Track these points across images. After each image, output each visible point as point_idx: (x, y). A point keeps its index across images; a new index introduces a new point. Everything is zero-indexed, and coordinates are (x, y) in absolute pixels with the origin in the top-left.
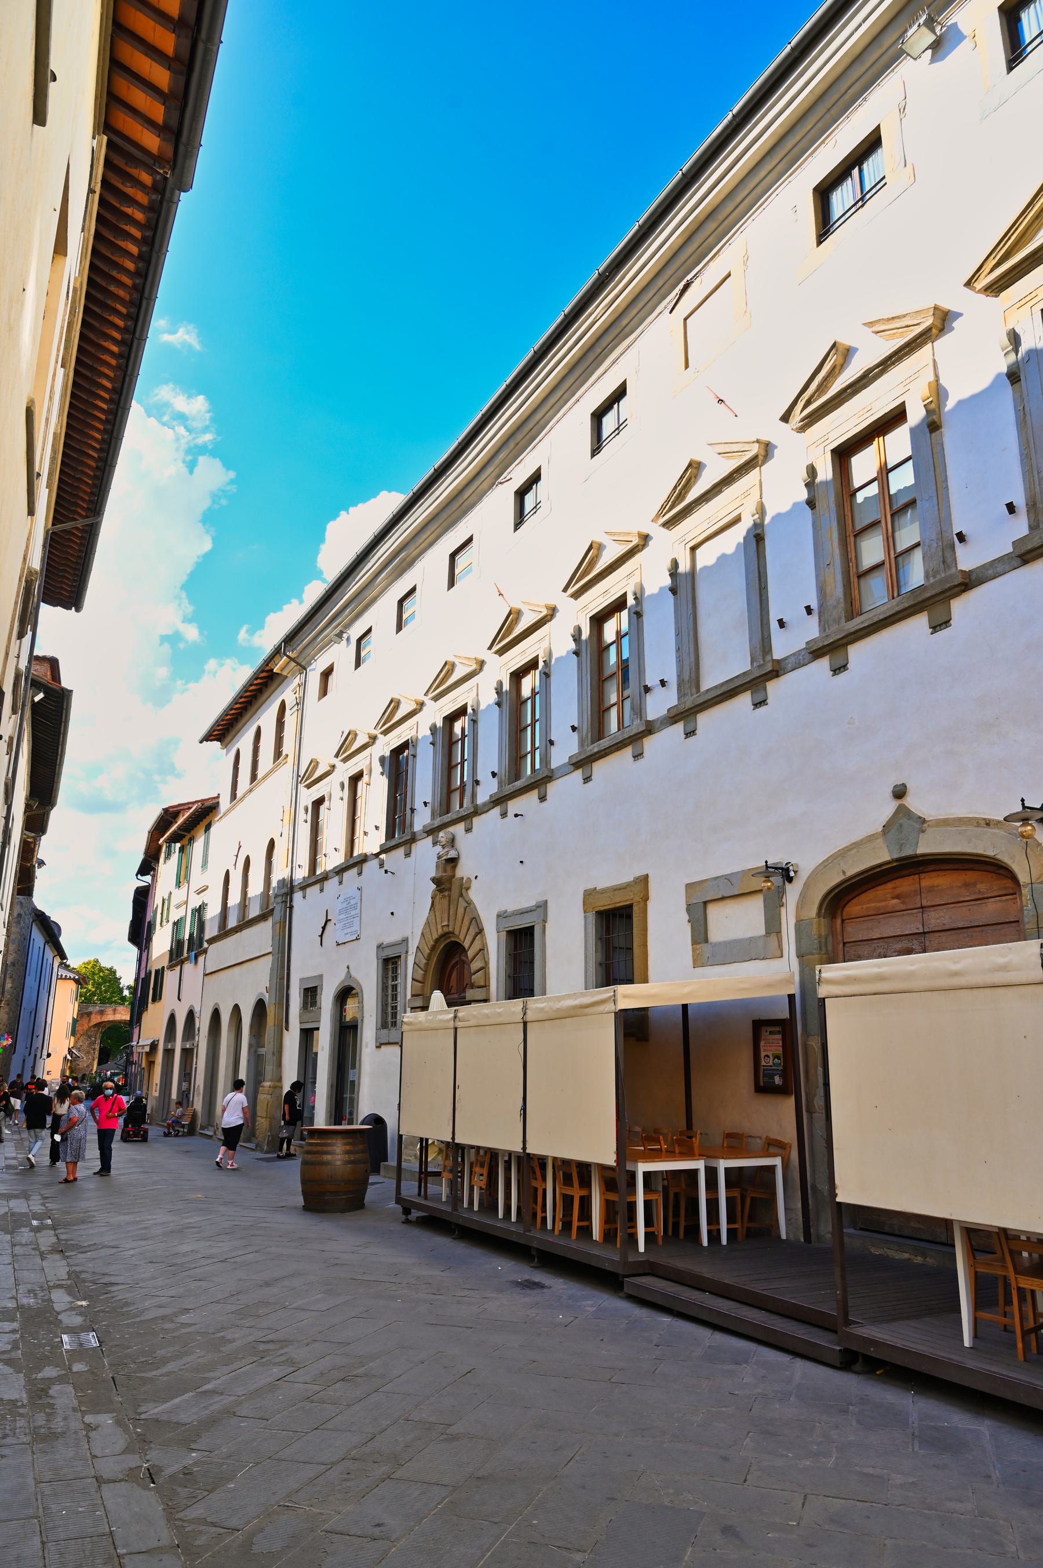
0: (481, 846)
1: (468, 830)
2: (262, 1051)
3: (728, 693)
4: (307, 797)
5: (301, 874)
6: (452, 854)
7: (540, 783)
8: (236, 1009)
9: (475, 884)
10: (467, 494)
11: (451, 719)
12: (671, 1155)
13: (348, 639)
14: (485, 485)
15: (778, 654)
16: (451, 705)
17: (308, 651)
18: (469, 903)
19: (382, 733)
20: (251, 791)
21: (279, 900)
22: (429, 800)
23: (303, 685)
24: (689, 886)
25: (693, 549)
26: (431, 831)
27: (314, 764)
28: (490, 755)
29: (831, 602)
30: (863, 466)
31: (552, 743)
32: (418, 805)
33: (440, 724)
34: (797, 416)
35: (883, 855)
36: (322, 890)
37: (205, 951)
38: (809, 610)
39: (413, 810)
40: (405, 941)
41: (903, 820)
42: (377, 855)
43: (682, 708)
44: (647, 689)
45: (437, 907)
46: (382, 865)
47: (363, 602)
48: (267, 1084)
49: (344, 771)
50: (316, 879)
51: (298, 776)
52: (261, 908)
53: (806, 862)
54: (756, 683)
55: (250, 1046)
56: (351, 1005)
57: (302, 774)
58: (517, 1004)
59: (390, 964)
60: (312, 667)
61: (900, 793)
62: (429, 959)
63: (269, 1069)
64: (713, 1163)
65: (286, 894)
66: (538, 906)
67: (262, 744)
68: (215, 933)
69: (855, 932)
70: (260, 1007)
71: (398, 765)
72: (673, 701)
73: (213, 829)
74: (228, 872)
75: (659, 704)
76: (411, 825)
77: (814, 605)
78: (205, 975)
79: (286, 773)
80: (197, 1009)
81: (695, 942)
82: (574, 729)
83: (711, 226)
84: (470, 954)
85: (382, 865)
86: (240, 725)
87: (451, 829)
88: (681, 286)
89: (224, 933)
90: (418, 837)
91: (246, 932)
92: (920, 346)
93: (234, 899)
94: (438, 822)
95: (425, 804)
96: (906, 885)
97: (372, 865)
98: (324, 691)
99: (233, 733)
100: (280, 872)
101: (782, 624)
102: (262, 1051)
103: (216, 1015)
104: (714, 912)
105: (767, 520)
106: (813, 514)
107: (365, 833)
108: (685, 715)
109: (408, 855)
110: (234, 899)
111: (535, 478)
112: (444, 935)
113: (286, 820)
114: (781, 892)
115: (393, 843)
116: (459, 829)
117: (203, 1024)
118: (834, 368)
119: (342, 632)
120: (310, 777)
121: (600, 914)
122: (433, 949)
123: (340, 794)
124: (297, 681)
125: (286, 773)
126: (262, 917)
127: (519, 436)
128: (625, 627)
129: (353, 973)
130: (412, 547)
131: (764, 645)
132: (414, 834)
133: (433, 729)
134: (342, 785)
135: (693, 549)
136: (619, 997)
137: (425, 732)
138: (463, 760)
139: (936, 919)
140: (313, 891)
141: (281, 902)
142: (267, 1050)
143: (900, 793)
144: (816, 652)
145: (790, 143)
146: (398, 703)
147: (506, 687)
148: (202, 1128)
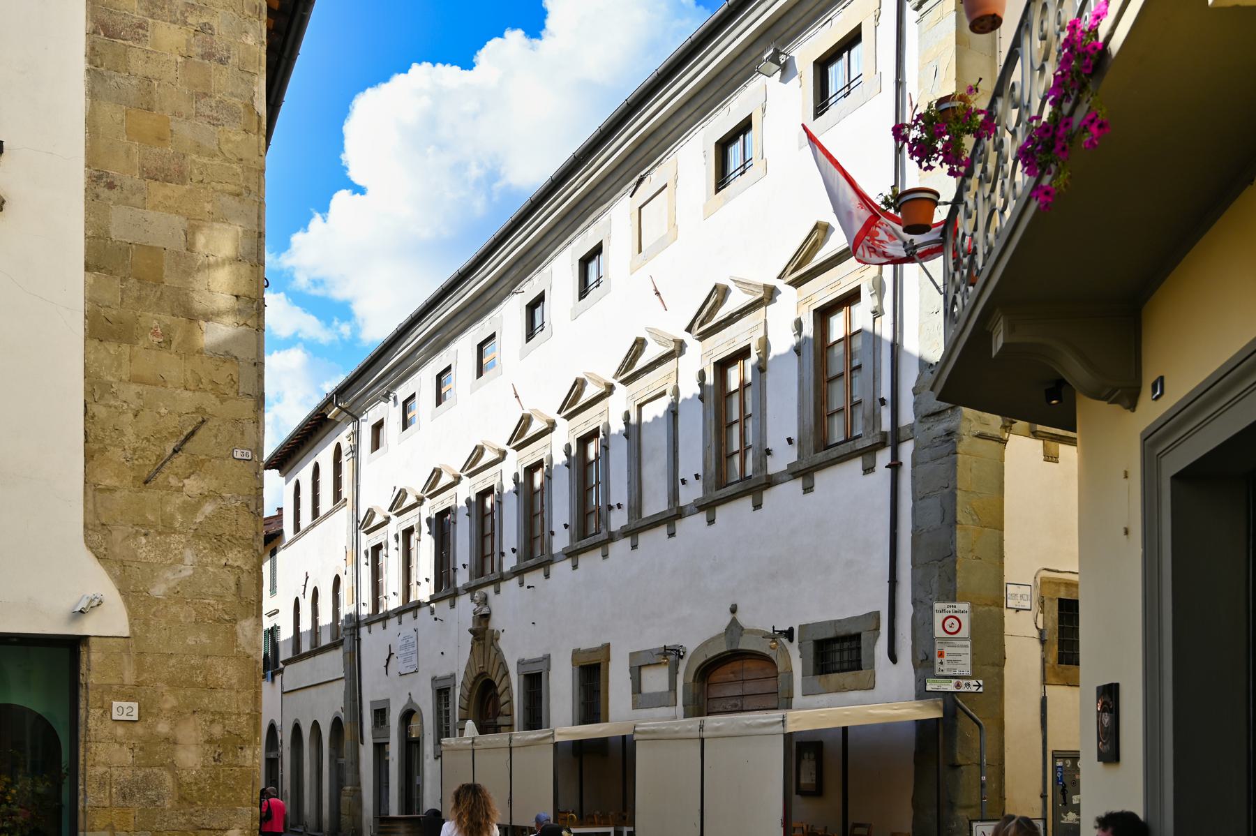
0: (509, 604)
1: (497, 592)
2: (342, 761)
3: (654, 523)
4: (367, 542)
5: (365, 611)
6: (485, 611)
7: (545, 564)
8: (316, 725)
9: (502, 636)
10: (489, 296)
11: (584, 441)
12: (600, 825)
13: (395, 398)
14: (503, 292)
15: (682, 503)
16: (583, 427)
17: (358, 404)
18: (498, 651)
19: (622, 382)
20: (314, 526)
21: (348, 632)
22: (467, 562)
23: (356, 433)
24: (631, 654)
25: (640, 406)
26: (470, 590)
27: (371, 513)
28: (561, 511)
29: (709, 474)
30: (838, 327)
31: (768, 452)
32: (459, 566)
33: (473, 499)
34: (697, 330)
35: (723, 648)
36: (415, 617)
37: (281, 671)
38: (790, 441)
39: (455, 570)
40: (453, 676)
41: (734, 628)
42: (428, 604)
43: (632, 527)
44: (610, 508)
45: (475, 652)
46: (432, 612)
47: (407, 369)
48: (348, 788)
49: (397, 525)
50: (379, 618)
51: (358, 521)
52: (332, 638)
53: (690, 646)
54: (671, 518)
55: (331, 756)
56: (414, 724)
57: (361, 518)
58: (696, 721)
59: (442, 694)
60: (364, 417)
61: (734, 610)
62: (471, 691)
63: (349, 776)
64: (620, 829)
65: (353, 628)
66: (544, 658)
67: (302, 496)
68: (289, 655)
69: (714, 692)
70: (337, 723)
71: (442, 525)
72: (625, 522)
73: (280, 555)
74: (297, 599)
75: (618, 520)
76: (550, 548)
77: (701, 473)
78: (283, 693)
79: (344, 514)
80: (278, 723)
81: (633, 693)
82: (566, 526)
83: (652, 142)
84: (500, 690)
85: (432, 612)
86: (298, 457)
87: (484, 590)
88: (637, 178)
89: (298, 656)
90: (557, 559)
91: (319, 658)
92: (760, 307)
93: (306, 625)
94: (473, 583)
95: (464, 566)
96: (736, 665)
97: (424, 612)
98: (376, 445)
99: (310, 445)
100: (346, 609)
101: (683, 482)
102: (342, 761)
103: (297, 729)
104: (646, 673)
105: (771, 357)
106: (799, 361)
107: (418, 583)
108: (631, 533)
109: (452, 606)
110: (306, 625)
111: (745, 126)
112: (482, 674)
113: (349, 560)
114: (677, 665)
115: (440, 595)
116: (490, 590)
117: (285, 737)
118: (716, 302)
119: (389, 393)
120: (365, 524)
121: (582, 668)
122: (474, 684)
123: (395, 545)
124: (350, 428)
125: (343, 517)
126: (334, 646)
127: (527, 261)
128: (749, 378)
129: (414, 699)
130: (445, 332)
131: (674, 495)
132: (456, 589)
133: (468, 501)
134: (397, 537)
135: (640, 406)
136: (788, 719)
137: (461, 503)
138: (598, 483)
139: (750, 687)
140: (377, 627)
141: (348, 634)
142: (346, 759)
143: (734, 610)
144: (701, 508)
145: (700, 101)
146: (373, 515)
147: (522, 479)
148: (292, 826)
